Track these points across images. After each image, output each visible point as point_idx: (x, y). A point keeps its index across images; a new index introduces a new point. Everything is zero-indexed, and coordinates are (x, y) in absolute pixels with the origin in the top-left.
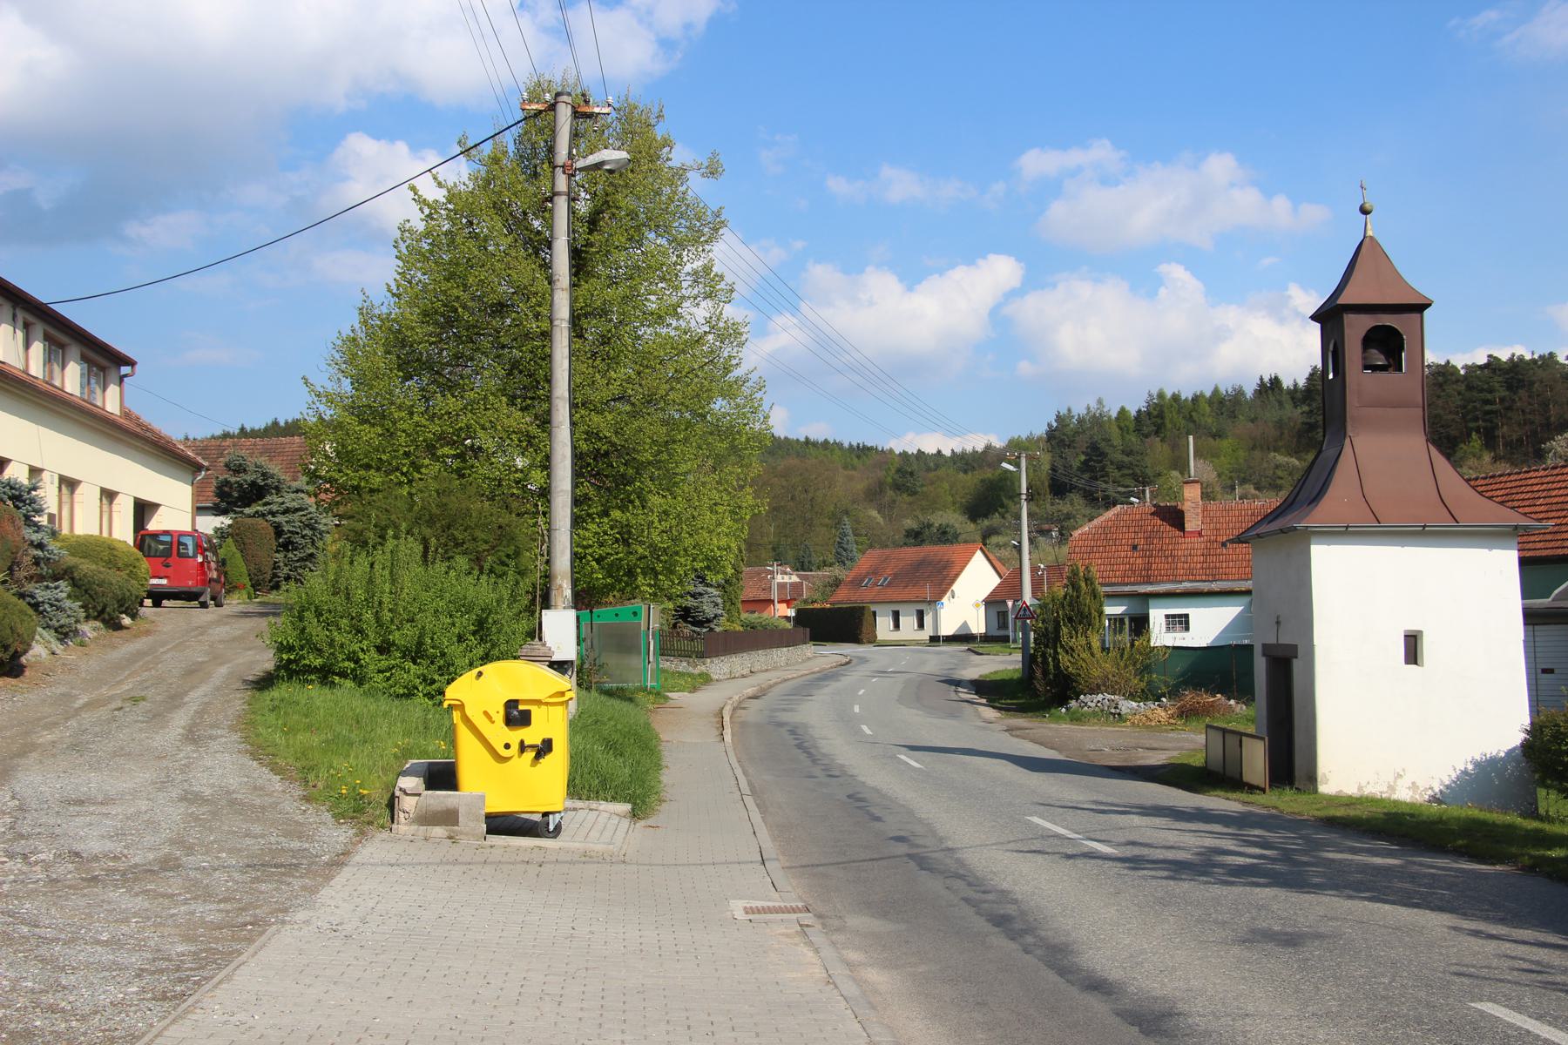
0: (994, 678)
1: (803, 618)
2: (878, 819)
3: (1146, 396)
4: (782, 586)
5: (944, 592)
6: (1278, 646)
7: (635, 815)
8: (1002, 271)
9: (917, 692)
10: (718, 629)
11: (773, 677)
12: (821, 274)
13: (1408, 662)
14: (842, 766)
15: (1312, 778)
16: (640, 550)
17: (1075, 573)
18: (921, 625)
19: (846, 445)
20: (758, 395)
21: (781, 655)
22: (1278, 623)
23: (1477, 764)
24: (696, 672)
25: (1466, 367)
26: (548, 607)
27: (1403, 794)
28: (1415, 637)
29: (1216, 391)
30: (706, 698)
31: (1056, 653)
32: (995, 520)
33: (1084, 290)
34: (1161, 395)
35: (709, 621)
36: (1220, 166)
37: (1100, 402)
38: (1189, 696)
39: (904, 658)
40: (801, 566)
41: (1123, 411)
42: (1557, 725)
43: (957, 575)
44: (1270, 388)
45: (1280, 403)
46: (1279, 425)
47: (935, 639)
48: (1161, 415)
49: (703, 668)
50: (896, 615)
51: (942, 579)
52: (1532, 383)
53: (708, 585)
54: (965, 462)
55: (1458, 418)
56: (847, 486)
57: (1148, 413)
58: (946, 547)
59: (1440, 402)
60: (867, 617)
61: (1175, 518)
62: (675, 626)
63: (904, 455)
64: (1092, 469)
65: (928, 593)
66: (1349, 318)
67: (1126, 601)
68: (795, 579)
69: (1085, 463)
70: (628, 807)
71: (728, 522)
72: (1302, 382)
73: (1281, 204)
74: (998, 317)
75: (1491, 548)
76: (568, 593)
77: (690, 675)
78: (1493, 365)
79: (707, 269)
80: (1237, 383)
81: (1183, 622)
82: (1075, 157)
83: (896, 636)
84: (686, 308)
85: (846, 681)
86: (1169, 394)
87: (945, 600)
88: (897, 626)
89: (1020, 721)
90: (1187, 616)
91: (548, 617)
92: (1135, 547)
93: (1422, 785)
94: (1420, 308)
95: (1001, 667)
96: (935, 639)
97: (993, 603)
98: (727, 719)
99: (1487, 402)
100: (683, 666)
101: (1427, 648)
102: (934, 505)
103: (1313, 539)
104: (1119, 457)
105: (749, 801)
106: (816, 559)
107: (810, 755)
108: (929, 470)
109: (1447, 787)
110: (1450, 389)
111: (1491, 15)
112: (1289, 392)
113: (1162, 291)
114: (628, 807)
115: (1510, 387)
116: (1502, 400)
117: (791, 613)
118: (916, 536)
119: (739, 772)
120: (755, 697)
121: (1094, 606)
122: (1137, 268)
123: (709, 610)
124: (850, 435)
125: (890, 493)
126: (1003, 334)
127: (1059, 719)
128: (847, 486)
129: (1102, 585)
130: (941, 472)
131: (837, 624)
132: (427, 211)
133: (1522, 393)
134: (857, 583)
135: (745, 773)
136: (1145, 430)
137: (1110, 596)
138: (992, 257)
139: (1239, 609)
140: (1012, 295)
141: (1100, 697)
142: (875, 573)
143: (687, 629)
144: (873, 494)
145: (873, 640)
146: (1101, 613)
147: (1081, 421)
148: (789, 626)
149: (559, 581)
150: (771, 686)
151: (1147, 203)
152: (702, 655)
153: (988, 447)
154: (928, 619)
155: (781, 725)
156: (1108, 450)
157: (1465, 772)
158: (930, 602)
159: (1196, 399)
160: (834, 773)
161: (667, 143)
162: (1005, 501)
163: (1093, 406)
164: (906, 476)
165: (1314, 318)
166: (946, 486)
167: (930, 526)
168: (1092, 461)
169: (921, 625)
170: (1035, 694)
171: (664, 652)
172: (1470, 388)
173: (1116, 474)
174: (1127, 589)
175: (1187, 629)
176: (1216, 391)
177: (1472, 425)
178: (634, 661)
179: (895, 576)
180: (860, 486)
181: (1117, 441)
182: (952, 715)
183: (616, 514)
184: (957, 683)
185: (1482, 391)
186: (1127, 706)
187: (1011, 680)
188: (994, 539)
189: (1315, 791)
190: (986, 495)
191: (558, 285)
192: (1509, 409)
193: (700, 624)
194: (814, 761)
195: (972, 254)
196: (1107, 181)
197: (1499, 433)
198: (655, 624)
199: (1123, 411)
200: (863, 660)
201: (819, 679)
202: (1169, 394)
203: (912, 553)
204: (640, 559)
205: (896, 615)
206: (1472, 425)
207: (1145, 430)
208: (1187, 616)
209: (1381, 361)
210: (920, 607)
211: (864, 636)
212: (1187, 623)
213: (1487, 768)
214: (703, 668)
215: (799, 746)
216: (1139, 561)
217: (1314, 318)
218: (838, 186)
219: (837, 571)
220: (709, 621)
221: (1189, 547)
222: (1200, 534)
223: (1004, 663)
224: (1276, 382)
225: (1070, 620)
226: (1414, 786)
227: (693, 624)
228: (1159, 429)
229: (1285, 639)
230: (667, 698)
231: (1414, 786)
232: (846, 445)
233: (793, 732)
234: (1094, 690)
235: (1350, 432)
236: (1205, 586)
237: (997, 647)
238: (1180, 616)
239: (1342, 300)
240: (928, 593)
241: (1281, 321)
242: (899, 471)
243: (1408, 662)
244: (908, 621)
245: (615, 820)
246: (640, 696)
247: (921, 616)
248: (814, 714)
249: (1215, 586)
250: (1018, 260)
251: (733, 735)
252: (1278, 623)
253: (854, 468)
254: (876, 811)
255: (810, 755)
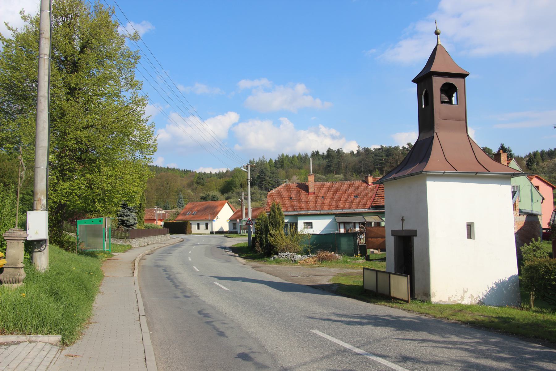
0: (237, 246)
1: (166, 225)
2: (222, 334)
3: (278, 156)
4: (159, 215)
5: (215, 217)
6: (403, 231)
7: (63, 343)
8: (233, 117)
9: (211, 251)
10: (135, 228)
11: (156, 246)
12: (174, 116)
13: (468, 238)
14: (190, 290)
15: (427, 294)
16: (97, 191)
17: (274, 206)
18: (207, 228)
19: (181, 170)
20: (152, 129)
21: (159, 238)
22: (403, 220)
23: (497, 285)
24: (126, 244)
25: (374, 149)
26: (32, 209)
27: (466, 301)
28: (470, 225)
29: (299, 154)
30: (129, 255)
31: (266, 236)
32: (230, 194)
33: (258, 123)
34: (283, 155)
35: (132, 225)
36: (301, 88)
37: (263, 157)
38: (320, 253)
39: (203, 240)
40: (165, 208)
41: (271, 160)
42: (546, 266)
43: (219, 211)
44: (316, 154)
45: (319, 159)
46: (319, 165)
47: (212, 233)
48: (283, 162)
49: (129, 243)
50: (198, 225)
51: (214, 212)
52: (393, 154)
53: (132, 212)
54: (220, 175)
55: (372, 164)
56: (181, 183)
57: (279, 161)
58: (215, 202)
59: (367, 159)
60: (189, 225)
61: (305, 188)
62: (118, 227)
63: (200, 173)
64: (261, 178)
65: (209, 217)
66: (435, 79)
67: (289, 217)
68: (163, 212)
69: (259, 176)
70: (59, 337)
71: (138, 181)
72: (325, 153)
73: (318, 101)
74: (231, 132)
75: (501, 184)
76: (44, 202)
77: (124, 246)
78: (382, 149)
79: (132, 78)
80: (306, 152)
81: (310, 225)
82: (256, 83)
83: (198, 232)
84: (122, 94)
85: (183, 248)
86: (285, 155)
87: (215, 219)
88: (199, 228)
89: (255, 263)
90: (311, 223)
91: (31, 217)
92: (291, 198)
93: (475, 295)
94: (464, 76)
95: (240, 242)
96: (212, 233)
97: (232, 221)
98: (136, 264)
99: (380, 160)
100: (121, 242)
101: (477, 230)
102: (209, 189)
103: (427, 178)
104: (270, 174)
105: (143, 320)
106: (171, 206)
107: (174, 283)
108: (208, 177)
109: (485, 296)
110: (370, 155)
111: (374, 51)
112: (321, 156)
113: (281, 126)
114: (59, 337)
115: (387, 156)
116: (385, 159)
117: (162, 223)
118: (204, 199)
119: (139, 296)
120: (149, 254)
121: (280, 219)
122: (274, 117)
123: (132, 221)
124: (182, 167)
125: (195, 185)
126: (232, 135)
127: (271, 262)
128: (181, 183)
129: (285, 211)
130: (212, 178)
131: (178, 228)
132: (5, 44)
133: (390, 157)
134: (185, 214)
135: (143, 296)
136: (278, 166)
137: (286, 215)
138: (229, 113)
139: (331, 220)
140: (235, 124)
141: (287, 253)
142: (191, 210)
143: (123, 228)
144: (190, 185)
145: (190, 233)
146: (283, 222)
147: (257, 163)
148: (162, 228)
149: (39, 196)
150: (155, 250)
151: (278, 99)
152: (128, 238)
153: (227, 171)
154: (209, 226)
155: (159, 267)
156: (266, 172)
157: (492, 289)
158: (210, 220)
159: (293, 157)
160: (188, 295)
161: (116, 25)
162: (233, 188)
163: (261, 158)
164: (201, 180)
165: (413, 81)
166: (214, 183)
167: (209, 195)
168: (264, 176)
169: (207, 228)
170: (256, 252)
171: (113, 236)
172: (376, 155)
173: (269, 179)
174: (289, 213)
175: (312, 228)
176: (299, 154)
177: (376, 167)
178: (99, 240)
179: (198, 211)
180: (185, 183)
181: (269, 169)
182: (229, 262)
183: (88, 176)
184: (225, 248)
185: (379, 156)
186: (298, 257)
187: (244, 247)
188: (230, 200)
189: (429, 301)
190: (228, 186)
191: (43, 36)
192: (387, 162)
193: (128, 226)
194: (176, 287)
195: (223, 111)
196: (267, 90)
197: (384, 169)
198: (108, 225)
199: (271, 160)
200: (188, 240)
201: (173, 247)
202: (285, 155)
203: (204, 203)
204: (97, 195)
205: (198, 225)
206: (376, 167)
207: (278, 166)
208: (311, 223)
209: (447, 100)
210: (207, 222)
211: (187, 232)
212: (312, 225)
213: (501, 286)
214: (129, 243)
215: (168, 278)
216: (293, 203)
217: (413, 81)
218: (181, 87)
219: (178, 209)
220: (132, 225)
221: (310, 198)
222: (314, 194)
223: (242, 240)
224: (317, 152)
225: (272, 224)
226: (472, 296)
227: (126, 226)
228: (282, 166)
229: (408, 227)
230: (113, 255)
231: (472, 296)
232: (181, 170)
233: (165, 270)
234: (283, 251)
235: (436, 131)
236: (319, 212)
237: (235, 235)
238: (309, 223)
239: (434, 69)
240: (209, 217)
241: (318, 136)
242: (198, 178)
243: (468, 238)
244: (203, 227)
245: (48, 347)
246: (100, 256)
247: (207, 224)
248: (173, 261)
249: (322, 212)
250: (238, 114)
251: (139, 272)
252: (403, 220)
253: (183, 177)
254: (222, 328)
255: (174, 283)
